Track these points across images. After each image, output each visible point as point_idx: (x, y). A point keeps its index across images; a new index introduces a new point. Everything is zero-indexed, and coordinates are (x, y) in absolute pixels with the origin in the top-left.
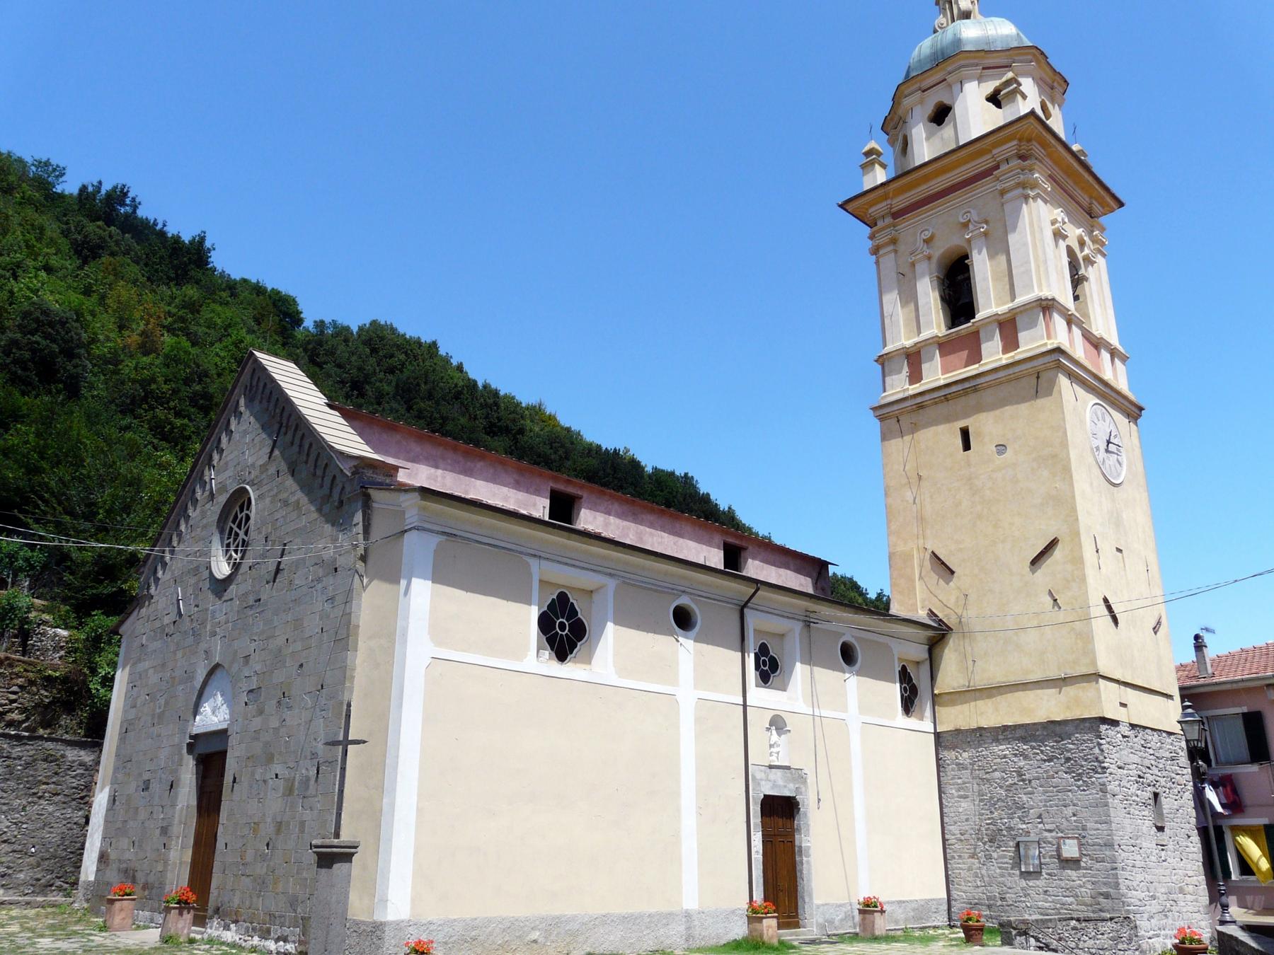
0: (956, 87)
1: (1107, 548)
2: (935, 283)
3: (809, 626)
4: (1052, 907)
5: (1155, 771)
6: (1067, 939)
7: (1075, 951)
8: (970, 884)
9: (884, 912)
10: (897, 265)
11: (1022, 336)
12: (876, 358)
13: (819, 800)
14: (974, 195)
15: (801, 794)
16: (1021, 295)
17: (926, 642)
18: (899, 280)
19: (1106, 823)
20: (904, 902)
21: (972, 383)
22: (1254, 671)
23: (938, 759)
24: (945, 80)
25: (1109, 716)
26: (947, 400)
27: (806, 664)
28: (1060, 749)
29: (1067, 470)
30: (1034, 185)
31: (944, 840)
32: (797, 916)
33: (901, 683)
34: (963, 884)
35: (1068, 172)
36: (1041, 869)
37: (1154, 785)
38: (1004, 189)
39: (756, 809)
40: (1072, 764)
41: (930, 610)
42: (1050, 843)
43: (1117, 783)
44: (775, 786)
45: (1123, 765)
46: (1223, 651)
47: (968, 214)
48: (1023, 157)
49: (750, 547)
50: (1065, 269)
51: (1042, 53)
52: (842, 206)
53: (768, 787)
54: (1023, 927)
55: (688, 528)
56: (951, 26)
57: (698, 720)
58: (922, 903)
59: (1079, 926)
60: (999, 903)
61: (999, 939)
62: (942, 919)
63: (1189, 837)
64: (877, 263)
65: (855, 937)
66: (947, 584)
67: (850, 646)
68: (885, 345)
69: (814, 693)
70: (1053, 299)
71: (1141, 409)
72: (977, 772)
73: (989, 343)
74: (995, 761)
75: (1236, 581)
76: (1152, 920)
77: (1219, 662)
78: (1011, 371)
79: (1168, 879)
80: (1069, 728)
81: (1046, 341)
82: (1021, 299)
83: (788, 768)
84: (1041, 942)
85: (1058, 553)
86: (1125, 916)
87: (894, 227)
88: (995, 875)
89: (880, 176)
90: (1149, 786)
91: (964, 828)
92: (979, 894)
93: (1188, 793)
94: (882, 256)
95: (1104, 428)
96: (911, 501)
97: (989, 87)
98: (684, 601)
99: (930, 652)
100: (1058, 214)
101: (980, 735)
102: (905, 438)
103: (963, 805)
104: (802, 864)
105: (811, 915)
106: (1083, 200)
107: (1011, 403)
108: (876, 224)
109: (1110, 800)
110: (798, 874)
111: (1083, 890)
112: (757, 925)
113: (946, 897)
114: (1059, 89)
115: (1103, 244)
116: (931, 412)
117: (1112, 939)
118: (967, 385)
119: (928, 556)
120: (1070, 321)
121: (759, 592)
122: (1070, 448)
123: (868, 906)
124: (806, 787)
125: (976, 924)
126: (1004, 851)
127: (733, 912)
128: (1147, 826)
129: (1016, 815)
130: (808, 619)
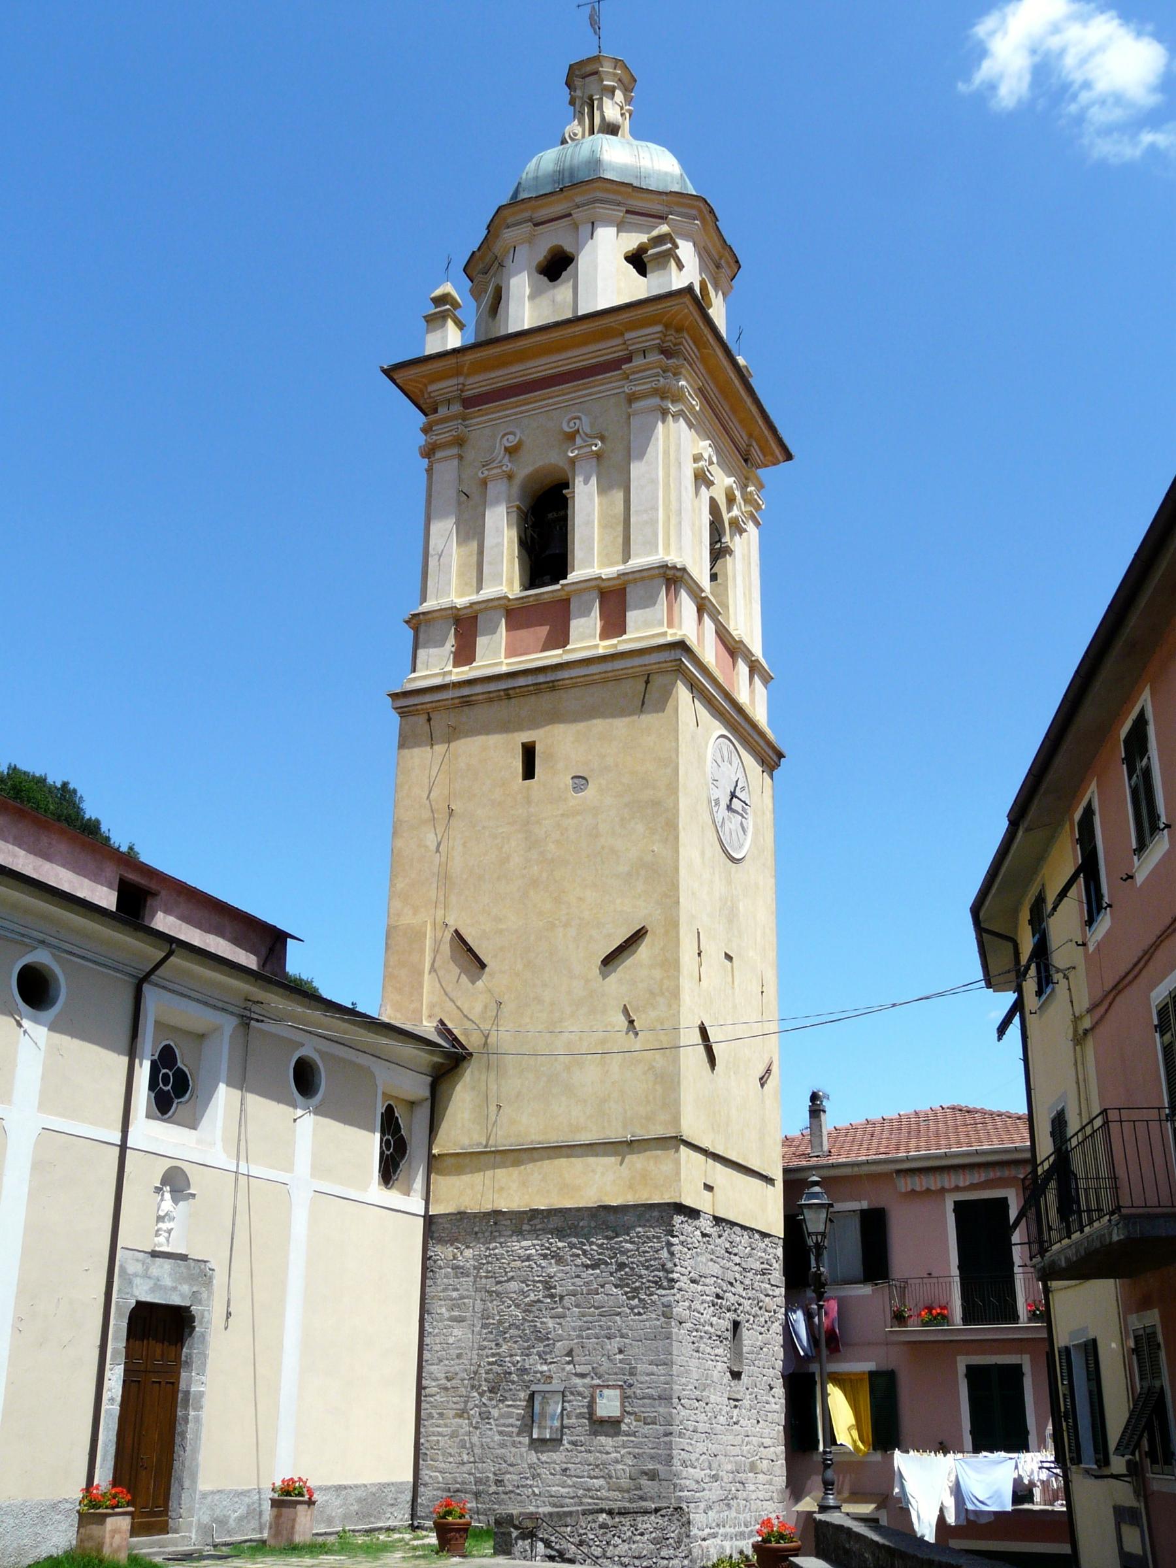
0: (585, 229)
1: (713, 953)
2: (514, 516)
3: (248, 1024)
4: (572, 1495)
5: (739, 1289)
6: (591, 1543)
7: (600, 1561)
8: (451, 1459)
9: (314, 1503)
10: (460, 480)
11: (632, 616)
12: (407, 617)
13: (229, 1314)
14: (591, 394)
15: (200, 1303)
16: (638, 555)
17: (428, 1070)
18: (459, 503)
19: (665, 1364)
20: (345, 1488)
21: (550, 677)
22: (882, 1150)
23: (425, 1258)
24: (570, 215)
25: (688, 1202)
26: (509, 697)
27: (234, 1087)
28: (612, 1248)
29: (672, 826)
30: (677, 398)
31: (420, 1388)
32: (166, 1512)
33: (383, 1133)
34: (441, 1458)
35: (725, 390)
36: (562, 1435)
37: (735, 1310)
38: (634, 393)
39: (119, 1325)
40: (626, 1274)
41: (442, 1022)
42: (580, 1394)
43: (687, 1304)
44: (157, 1287)
45: (698, 1278)
46: (843, 1124)
47: (577, 421)
48: (667, 353)
49: (163, 893)
50: (703, 528)
51: (712, 211)
52: (389, 373)
53: (146, 1288)
54: (529, 1524)
55: (63, 847)
56: (589, 139)
57: (38, 1166)
58: (374, 1490)
59: (610, 1522)
60: (493, 1489)
61: (492, 1543)
62: (400, 1516)
63: (771, 1388)
64: (430, 471)
65: (260, 1548)
66: (473, 982)
67: (311, 1066)
68: (424, 599)
69: (243, 1137)
70: (684, 570)
71: (781, 755)
72: (484, 1281)
73: (583, 620)
74: (513, 1264)
75: (894, 1005)
76: (710, 1513)
77: (837, 1137)
78: (609, 666)
79: (736, 1450)
80: (629, 1218)
81: (665, 629)
82: (638, 561)
83: (183, 1258)
84: (552, 1548)
85: (644, 951)
86: (676, 1506)
87: (464, 420)
88: (492, 1445)
89: (452, 338)
90: (729, 1310)
91: (452, 1369)
92: (463, 1475)
93: (777, 1324)
94: (440, 460)
95: (730, 773)
96: (433, 847)
97: (633, 240)
98: (41, 957)
99: (434, 1087)
100: (705, 447)
101: (495, 1223)
102: (436, 747)
103: (456, 1332)
104: (186, 1421)
105: (191, 1510)
106: (742, 437)
107: (603, 715)
108: (435, 411)
109: (675, 1330)
110: (178, 1440)
111: (620, 1467)
112: (94, 1529)
113: (411, 1480)
114: (726, 271)
115: (758, 507)
116: (481, 713)
117: (654, 1542)
118: (541, 679)
119: (448, 935)
120: (703, 607)
121: (172, 959)
122: (680, 795)
123: (288, 1494)
124: (210, 1293)
125: (459, 1521)
126: (509, 1406)
127: (54, 1506)
128: (719, 1371)
129: (535, 1351)
130: (247, 1013)
